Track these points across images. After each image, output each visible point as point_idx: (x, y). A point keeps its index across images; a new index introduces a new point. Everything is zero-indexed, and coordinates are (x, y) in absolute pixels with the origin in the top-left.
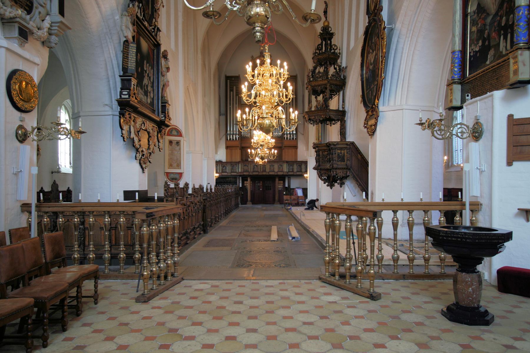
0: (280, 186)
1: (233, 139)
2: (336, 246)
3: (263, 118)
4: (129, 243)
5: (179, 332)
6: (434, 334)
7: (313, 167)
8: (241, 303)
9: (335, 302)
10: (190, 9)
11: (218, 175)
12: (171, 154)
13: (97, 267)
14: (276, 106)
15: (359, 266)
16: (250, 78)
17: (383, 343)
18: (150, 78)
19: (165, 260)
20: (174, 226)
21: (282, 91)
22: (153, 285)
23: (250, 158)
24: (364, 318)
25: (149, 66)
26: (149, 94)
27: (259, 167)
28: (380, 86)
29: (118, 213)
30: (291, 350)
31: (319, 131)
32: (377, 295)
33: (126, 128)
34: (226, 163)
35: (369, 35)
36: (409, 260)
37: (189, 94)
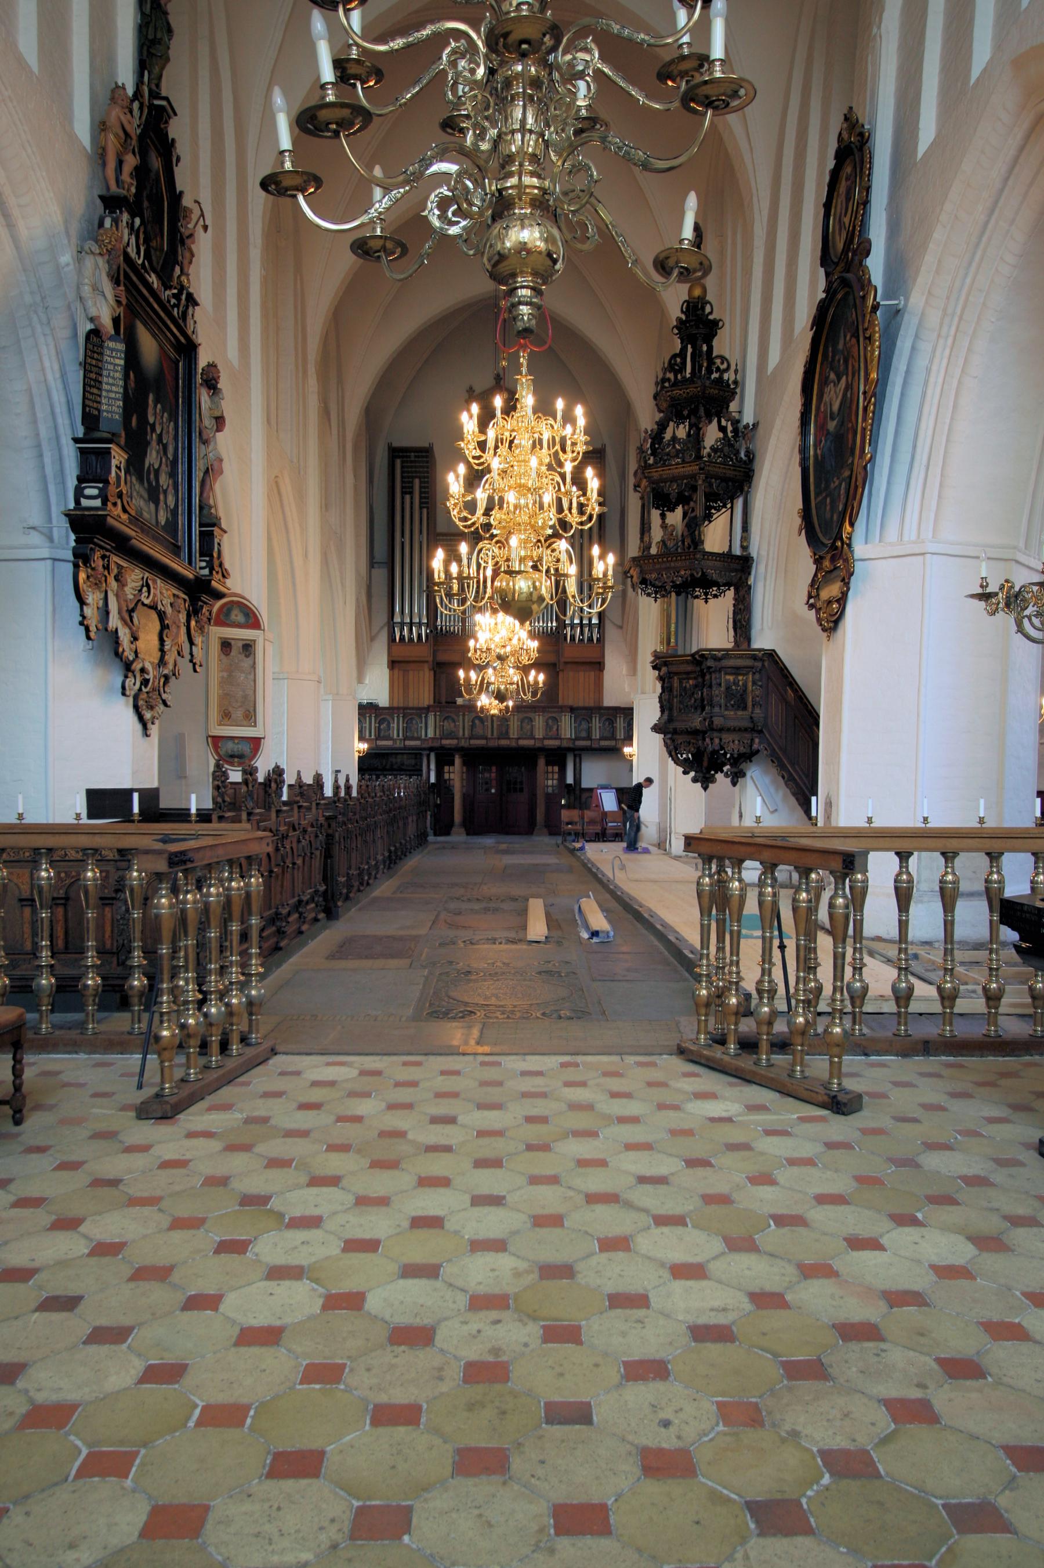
0: (550, 782)
1: (411, 640)
2: (732, 954)
3: (510, 573)
4: (108, 946)
5: (274, 1204)
6: (1021, 1211)
7: (652, 724)
8: (451, 1120)
9: (729, 1120)
10: (318, 226)
11: (364, 746)
12: (228, 680)
13: (21, 1015)
14: (550, 537)
15: (797, 1014)
16: (470, 450)
17: (873, 1235)
18: (165, 448)
19: (222, 995)
20: (248, 895)
21: (568, 493)
22: (189, 1068)
23: (461, 696)
24: (815, 1165)
25: (163, 410)
26: (162, 497)
27: (489, 724)
28: (860, 483)
29: (72, 855)
30: (605, 1256)
31: (669, 616)
32: (850, 1100)
33: (93, 598)
34: (391, 710)
35: (827, 326)
36: (943, 998)
37: (281, 501)
